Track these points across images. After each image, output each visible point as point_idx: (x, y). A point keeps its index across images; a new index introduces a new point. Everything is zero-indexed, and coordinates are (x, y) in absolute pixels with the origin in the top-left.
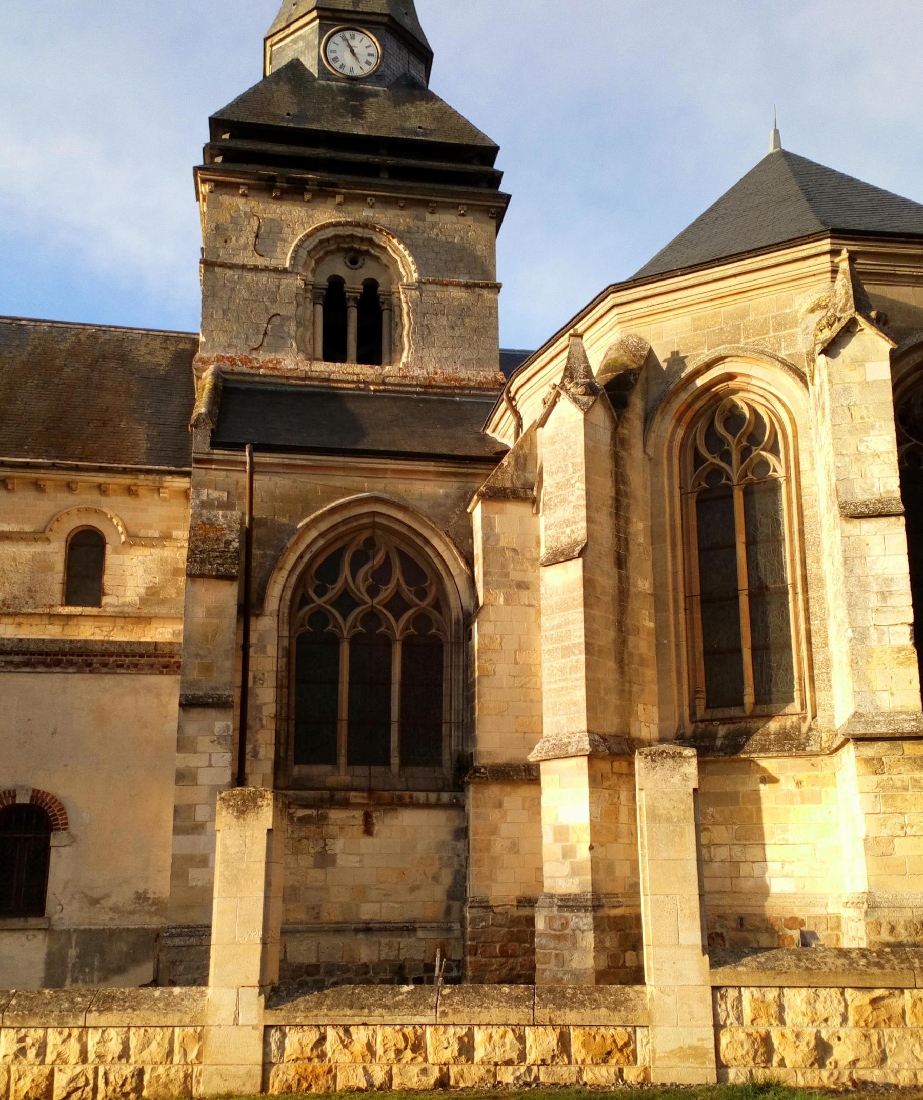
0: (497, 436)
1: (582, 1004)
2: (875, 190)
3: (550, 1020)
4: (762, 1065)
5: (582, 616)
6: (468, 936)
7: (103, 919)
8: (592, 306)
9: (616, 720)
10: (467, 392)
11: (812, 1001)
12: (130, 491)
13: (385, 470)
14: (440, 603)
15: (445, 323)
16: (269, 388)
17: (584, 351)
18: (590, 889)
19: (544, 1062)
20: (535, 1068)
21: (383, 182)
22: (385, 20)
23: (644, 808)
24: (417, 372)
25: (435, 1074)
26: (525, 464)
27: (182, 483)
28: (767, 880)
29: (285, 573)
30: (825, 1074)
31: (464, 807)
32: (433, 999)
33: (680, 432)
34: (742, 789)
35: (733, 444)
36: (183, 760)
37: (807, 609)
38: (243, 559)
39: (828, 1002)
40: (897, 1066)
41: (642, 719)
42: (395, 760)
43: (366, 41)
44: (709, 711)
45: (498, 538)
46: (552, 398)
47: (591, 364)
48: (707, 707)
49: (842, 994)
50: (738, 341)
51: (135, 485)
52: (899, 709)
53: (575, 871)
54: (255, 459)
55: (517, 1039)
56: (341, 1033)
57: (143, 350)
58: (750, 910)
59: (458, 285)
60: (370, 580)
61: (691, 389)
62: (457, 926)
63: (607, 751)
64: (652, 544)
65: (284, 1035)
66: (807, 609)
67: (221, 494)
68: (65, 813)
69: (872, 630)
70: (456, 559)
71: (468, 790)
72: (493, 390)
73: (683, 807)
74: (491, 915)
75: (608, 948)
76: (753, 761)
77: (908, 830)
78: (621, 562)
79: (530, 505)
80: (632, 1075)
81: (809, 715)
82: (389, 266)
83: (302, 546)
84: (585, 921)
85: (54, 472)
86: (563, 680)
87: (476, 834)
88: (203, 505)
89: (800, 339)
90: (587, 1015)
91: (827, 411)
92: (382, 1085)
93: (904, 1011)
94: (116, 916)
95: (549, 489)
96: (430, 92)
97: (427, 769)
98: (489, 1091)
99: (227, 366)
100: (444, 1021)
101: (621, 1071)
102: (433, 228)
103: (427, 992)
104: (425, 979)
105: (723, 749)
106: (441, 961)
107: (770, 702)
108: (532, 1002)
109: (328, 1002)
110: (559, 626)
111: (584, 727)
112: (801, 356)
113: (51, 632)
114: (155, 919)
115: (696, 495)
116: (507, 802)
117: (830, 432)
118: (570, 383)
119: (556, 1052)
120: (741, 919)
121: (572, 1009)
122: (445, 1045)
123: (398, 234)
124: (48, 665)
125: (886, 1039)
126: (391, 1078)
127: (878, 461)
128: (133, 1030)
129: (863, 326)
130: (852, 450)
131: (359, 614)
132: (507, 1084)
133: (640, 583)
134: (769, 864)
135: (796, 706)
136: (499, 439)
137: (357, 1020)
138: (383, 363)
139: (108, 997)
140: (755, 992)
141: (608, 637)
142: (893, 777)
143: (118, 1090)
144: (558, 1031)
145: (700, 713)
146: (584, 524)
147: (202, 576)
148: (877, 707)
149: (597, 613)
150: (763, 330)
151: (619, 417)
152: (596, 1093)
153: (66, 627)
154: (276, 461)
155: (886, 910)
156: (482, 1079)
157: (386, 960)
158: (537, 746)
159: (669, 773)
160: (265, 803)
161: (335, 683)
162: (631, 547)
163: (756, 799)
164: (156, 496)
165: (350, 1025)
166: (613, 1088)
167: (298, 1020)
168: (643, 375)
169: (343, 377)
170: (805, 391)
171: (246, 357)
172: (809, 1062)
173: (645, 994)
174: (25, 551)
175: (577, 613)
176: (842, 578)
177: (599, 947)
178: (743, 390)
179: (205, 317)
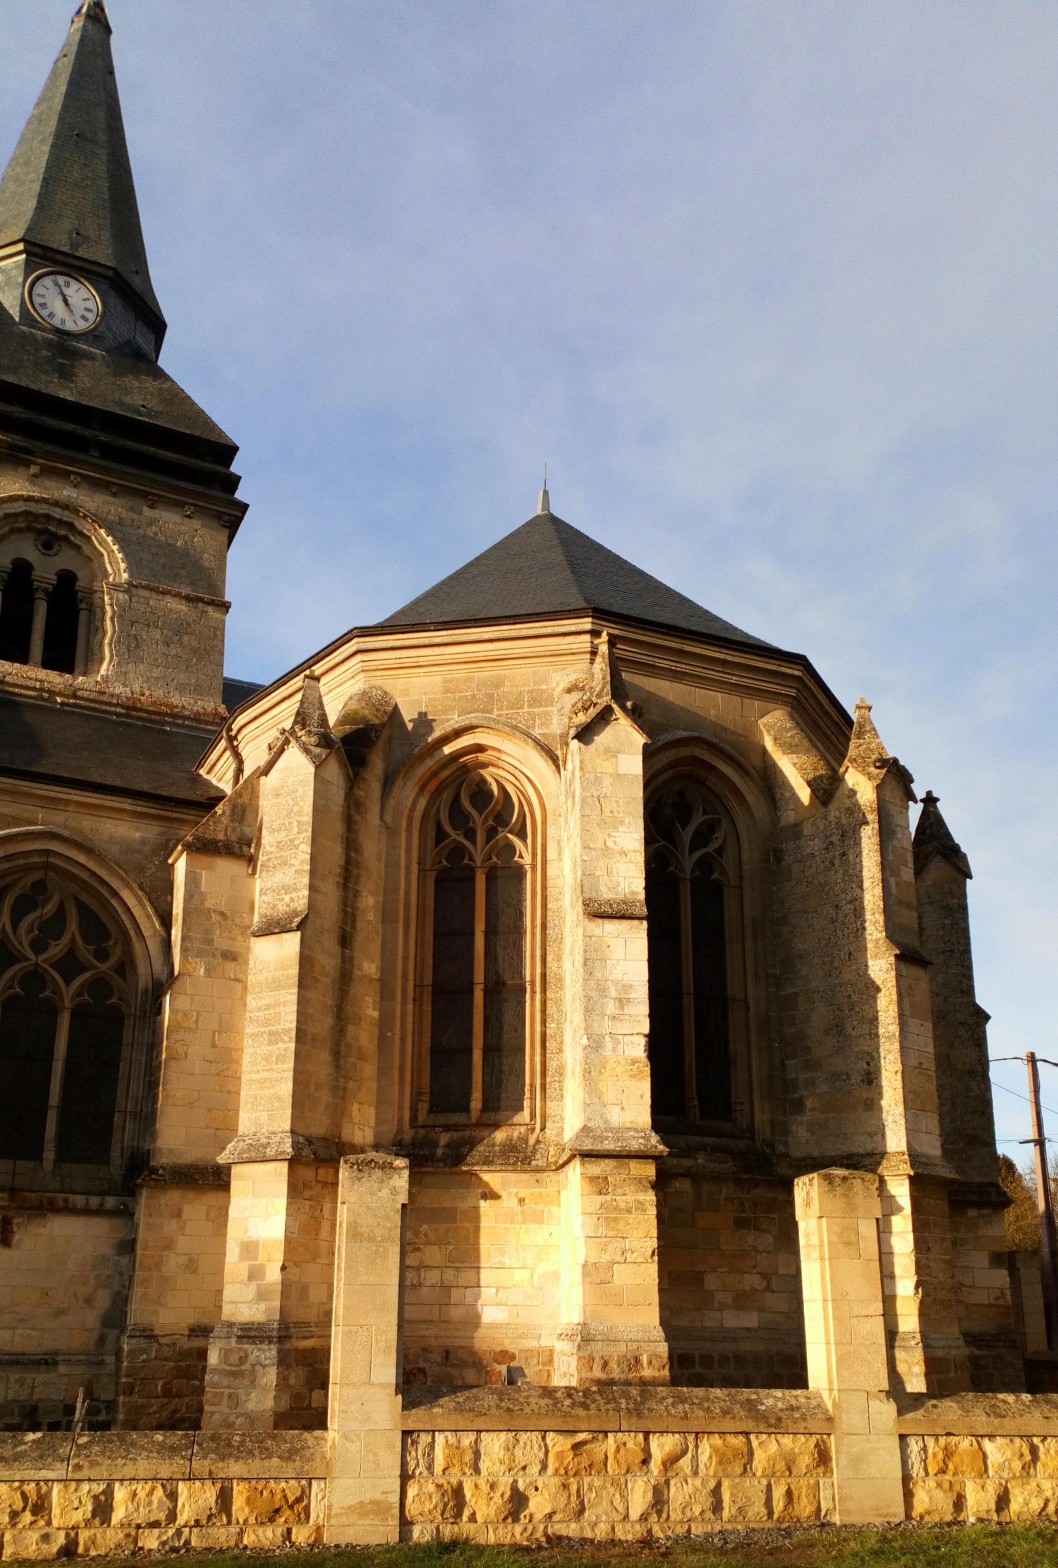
0: (213, 779)
1: (251, 1453)
2: (641, 573)
3: (210, 1473)
4: (451, 1520)
5: (294, 998)
6: (123, 1372)
8: (333, 647)
9: (326, 1120)
10: (180, 721)
11: (511, 1447)
13: (67, 802)
14: (126, 967)
15: (158, 637)
17: (320, 697)
18: (277, 1317)
19: (197, 1524)
20: (186, 1530)
21: (92, 460)
22: (110, 273)
23: (344, 1225)
24: (119, 689)
25: (60, 1539)
28: (480, 1307)
30: (518, 1529)
31: (133, 1215)
33: (423, 802)
34: (462, 1205)
35: (479, 822)
37: (544, 1011)
39: (528, 1448)
40: (594, 1518)
41: (356, 1120)
42: (49, 1154)
43: (84, 293)
44: (432, 1116)
45: (203, 897)
46: (279, 744)
47: (328, 712)
48: (430, 1111)
49: (544, 1438)
50: (491, 712)
52: (628, 1125)
53: (262, 1296)
55: (167, 1496)
58: (457, 1342)
59: (177, 595)
60: (37, 932)
61: (437, 756)
62: (110, 1359)
63: (312, 1156)
64: (383, 922)
66: (544, 1011)
69: (607, 1038)
70: (149, 917)
71: (141, 1194)
72: (212, 723)
73: (388, 1225)
75: (292, 1387)
76: (475, 1175)
77: (629, 1255)
78: (345, 940)
79: (245, 864)
80: (301, 1536)
81: (538, 1126)
82: (93, 559)
84: (268, 1354)
86: (267, 1070)
87: (146, 1248)
89: (555, 720)
90: (256, 1466)
91: (577, 800)
93: (606, 1457)
95: (268, 848)
96: (159, 367)
97: (89, 1167)
98: (126, 1560)
100: (77, 1476)
101: (289, 1531)
102: (151, 524)
103: (57, 1442)
104: (64, 1423)
105: (443, 1160)
106: (83, 1402)
107: (497, 1109)
108: (190, 1452)
110: (268, 1007)
111: (287, 1126)
112: (554, 736)
115: (435, 873)
116: (188, 1210)
117: (579, 823)
118: (302, 730)
119: (214, 1511)
120: (447, 1352)
121: (237, 1460)
122: (76, 1504)
123: (107, 523)
125: (586, 1488)
127: (625, 859)
129: (619, 716)
130: (599, 844)
131: (18, 971)
132: (150, 1550)
133: (366, 965)
134: (483, 1290)
135: (525, 1116)
136: (214, 782)
138: (76, 672)
140: (450, 1437)
141: (324, 1024)
142: (618, 1198)
144: (219, 1485)
145: (422, 1118)
146: (306, 893)
148: (606, 1122)
149: (312, 995)
150: (517, 704)
151: (356, 775)
152: (256, 1559)
155: (600, 1343)
156: (118, 1546)
157: (14, 1401)
158: (230, 1146)
159: (376, 1186)
162: (359, 925)
163: (475, 1216)
166: (277, 1552)
168: (386, 733)
169: (21, 682)
170: (557, 775)
172: (502, 1516)
173: (326, 1440)
175: (291, 994)
176: (581, 981)
177: (282, 1384)
178: (493, 765)
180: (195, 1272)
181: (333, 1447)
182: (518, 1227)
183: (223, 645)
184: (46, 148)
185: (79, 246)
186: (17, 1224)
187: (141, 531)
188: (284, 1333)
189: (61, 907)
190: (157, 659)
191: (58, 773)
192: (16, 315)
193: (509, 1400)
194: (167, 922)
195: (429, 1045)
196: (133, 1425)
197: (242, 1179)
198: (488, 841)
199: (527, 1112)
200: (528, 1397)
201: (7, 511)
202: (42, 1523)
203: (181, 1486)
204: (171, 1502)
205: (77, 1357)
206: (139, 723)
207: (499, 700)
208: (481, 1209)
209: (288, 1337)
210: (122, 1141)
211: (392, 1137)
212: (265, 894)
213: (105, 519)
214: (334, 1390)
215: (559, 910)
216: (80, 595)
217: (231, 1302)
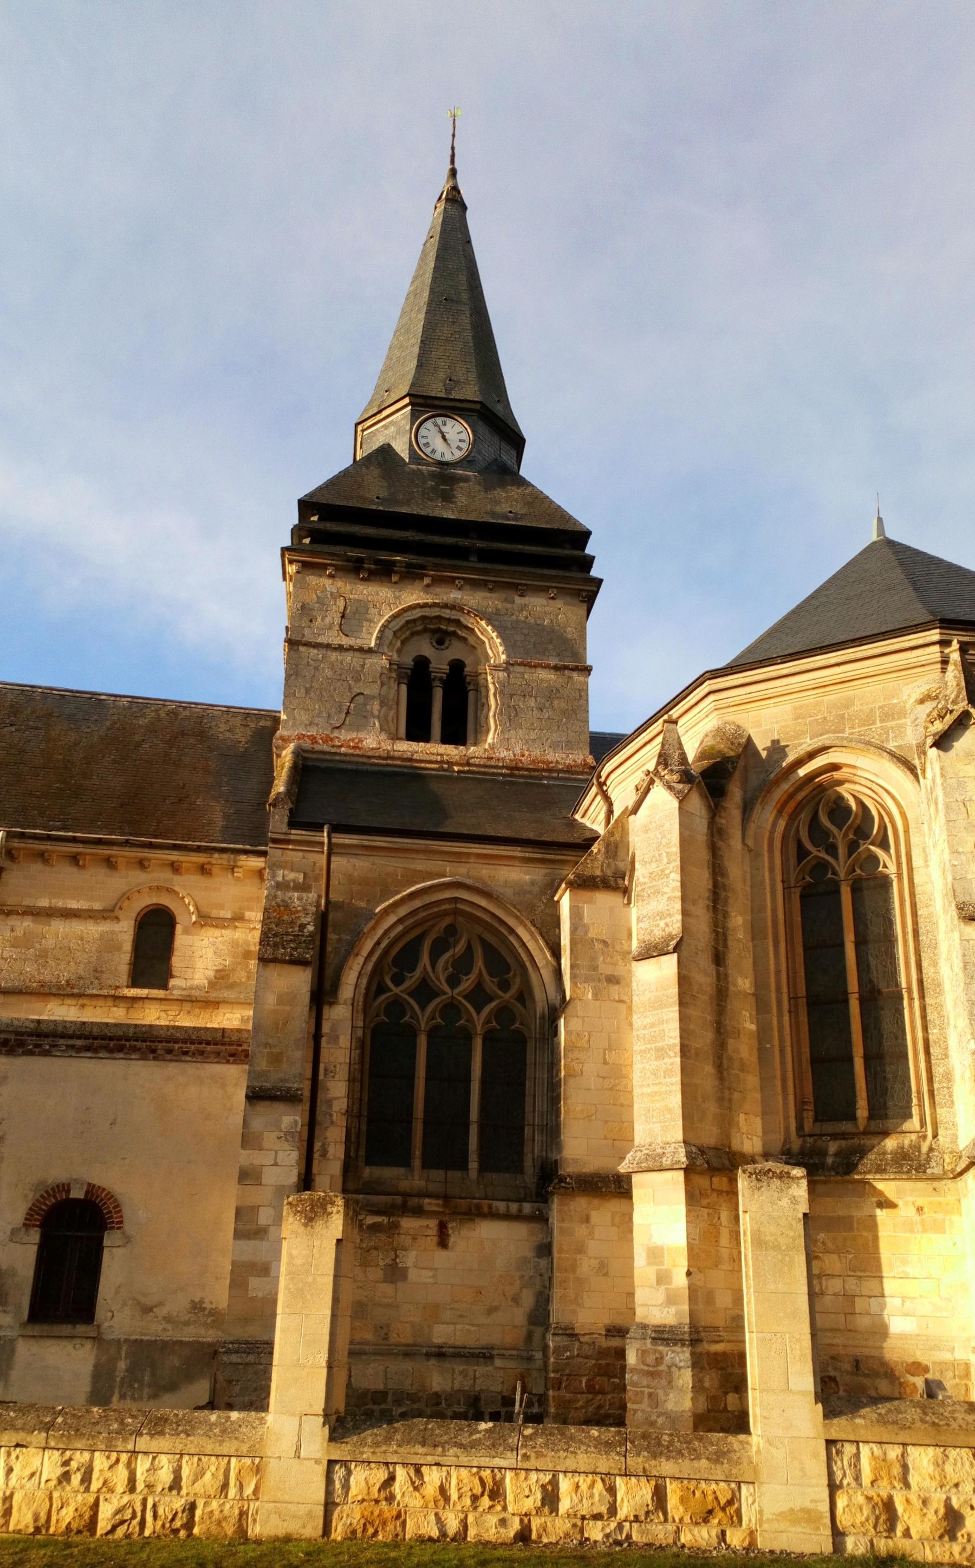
0: (587, 822)
1: (680, 1453)
5: (676, 1015)
6: (551, 1367)
7: (155, 1329)
8: (687, 691)
9: (715, 1131)
10: (555, 775)
11: (940, 1463)
12: (204, 870)
13: (469, 855)
14: (525, 996)
15: (533, 704)
16: (350, 767)
17: (679, 738)
18: (687, 1321)
20: (627, 1525)
21: (471, 565)
22: (478, 407)
24: (503, 754)
25: (515, 1525)
26: (616, 852)
27: (256, 863)
28: (886, 1317)
29: (361, 960)
30: (956, 1548)
31: (547, 1220)
32: (513, 1440)
33: (782, 823)
34: (857, 1214)
35: (840, 838)
36: (248, 1157)
37: (924, 1017)
38: (318, 943)
39: (959, 1464)
41: (744, 1130)
42: (473, 1165)
43: (458, 428)
44: (818, 1124)
45: (586, 928)
46: (645, 785)
48: (816, 1120)
50: (843, 731)
51: (209, 863)
53: (671, 1300)
54: (334, 840)
55: (607, 1490)
56: (412, 1473)
57: (223, 727)
58: (867, 1352)
59: (547, 667)
60: (451, 969)
61: (793, 778)
62: (538, 1355)
64: (753, 939)
65: (349, 1473)
66: (924, 1017)
67: (297, 875)
68: (120, 1211)
70: (541, 949)
71: (552, 1202)
72: (582, 773)
73: (792, 1234)
74: (577, 1344)
75: (707, 1389)
78: (719, 959)
79: (621, 895)
80: (736, 1539)
82: (476, 647)
83: (380, 932)
85: (127, 849)
87: (560, 1251)
88: (278, 886)
89: (909, 731)
90: (685, 1467)
91: (941, 806)
92: (456, 1535)
94: (169, 1327)
95: (641, 879)
97: (507, 1175)
98: (575, 1549)
99: (307, 744)
100: (526, 1465)
101: (723, 1533)
102: (522, 610)
105: (833, 1168)
109: (398, 1437)
110: (653, 1025)
111: (679, 1136)
113: (114, 1015)
114: (211, 1332)
116: (595, 1216)
117: (944, 828)
118: (664, 770)
119: (651, 1508)
121: (668, 1459)
122: (527, 1492)
124: (111, 1051)
126: (466, 1528)
128: (186, 1458)
131: (438, 1004)
132: (595, 1542)
133: (740, 981)
134: (888, 1300)
136: (589, 824)
137: (430, 1459)
139: (160, 1419)
140: (875, 1449)
141: (705, 1038)
143: (168, 1525)
144: (653, 1483)
146: (679, 917)
147: (275, 960)
149: (692, 1012)
150: (869, 720)
151: (716, 805)
153: (131, 1010)
154: (355, 842)
156: (567, 1535)
158: (628, 1156)
159: (776, 1194)
160: (335, 1209)
161: (411, 1078)
162: (730, 943)
163: (872, 1225)
164: (230, 876)
165: (422, 1465)
167: (365, 1456)
168: (741, 763)
170: (916, 784)
171: (327, 736)
173: (750, 1445)
174: (93, 929)
176: (962, 985)
177: (698, 1387)
179: (289, 694)
180: (606, 1274)
181: (758, 1452)
182: (918, 1236)
183: (588, 704)
184: (422, 316)
185: (451, 389)
186: (452, 1228)
187: (514, 617)
188: (695, 1336)
189: (469, 947)
190: (533, 724)
191: (458, 831)
192: (405, 456)
193: (934, 1414)
194: (557, 954)
195: (808, 1055)
196: (564, 1420)
197: (642, 1186)
198: (850, 855)
199: (916, 1119)
200: (953, 1412)
201: (408, 619)
202: (499, 1508)
203: (619, 1480)
204: (611, 1495)
205: (509, 1352)
206: (521, 780)
207: (850, 719)
208: (878, 1218)
209: (700, 1341)
210: (533, 1153)
211: (780, 1145)
212: (642, 921)
213: (485, 613)
214: (753, 1397)
215: (930, 915)
216: (468, 679)
217: (643, 1305)
